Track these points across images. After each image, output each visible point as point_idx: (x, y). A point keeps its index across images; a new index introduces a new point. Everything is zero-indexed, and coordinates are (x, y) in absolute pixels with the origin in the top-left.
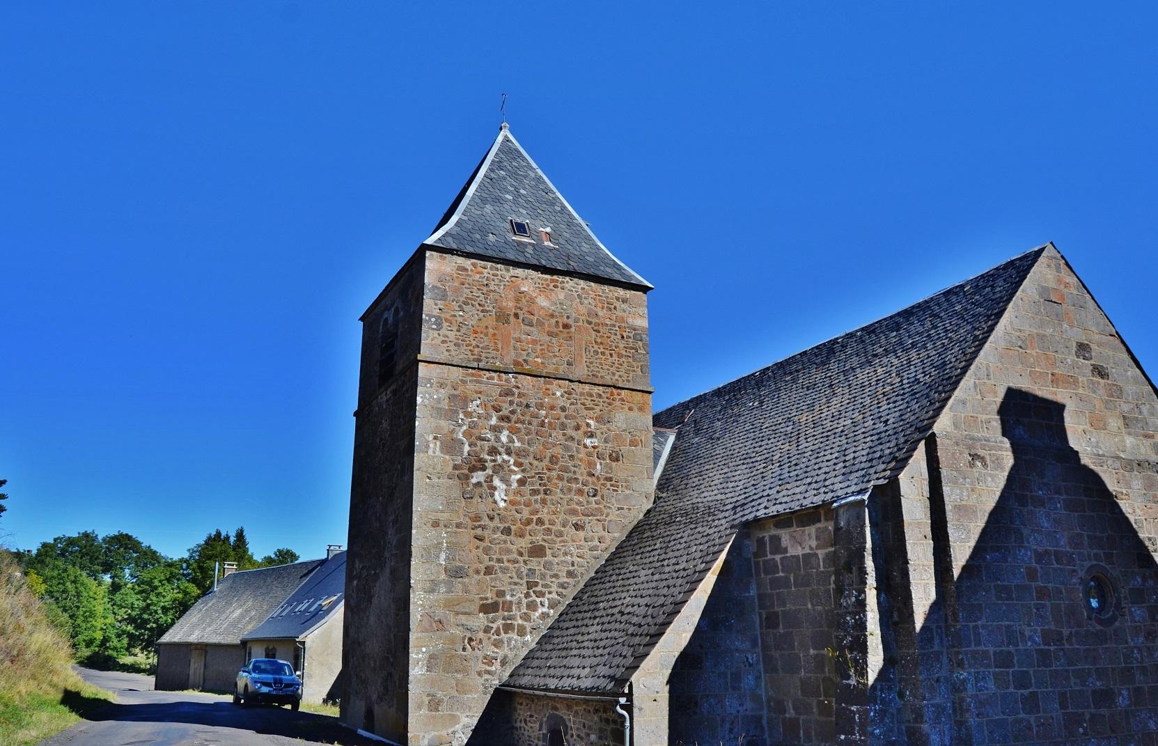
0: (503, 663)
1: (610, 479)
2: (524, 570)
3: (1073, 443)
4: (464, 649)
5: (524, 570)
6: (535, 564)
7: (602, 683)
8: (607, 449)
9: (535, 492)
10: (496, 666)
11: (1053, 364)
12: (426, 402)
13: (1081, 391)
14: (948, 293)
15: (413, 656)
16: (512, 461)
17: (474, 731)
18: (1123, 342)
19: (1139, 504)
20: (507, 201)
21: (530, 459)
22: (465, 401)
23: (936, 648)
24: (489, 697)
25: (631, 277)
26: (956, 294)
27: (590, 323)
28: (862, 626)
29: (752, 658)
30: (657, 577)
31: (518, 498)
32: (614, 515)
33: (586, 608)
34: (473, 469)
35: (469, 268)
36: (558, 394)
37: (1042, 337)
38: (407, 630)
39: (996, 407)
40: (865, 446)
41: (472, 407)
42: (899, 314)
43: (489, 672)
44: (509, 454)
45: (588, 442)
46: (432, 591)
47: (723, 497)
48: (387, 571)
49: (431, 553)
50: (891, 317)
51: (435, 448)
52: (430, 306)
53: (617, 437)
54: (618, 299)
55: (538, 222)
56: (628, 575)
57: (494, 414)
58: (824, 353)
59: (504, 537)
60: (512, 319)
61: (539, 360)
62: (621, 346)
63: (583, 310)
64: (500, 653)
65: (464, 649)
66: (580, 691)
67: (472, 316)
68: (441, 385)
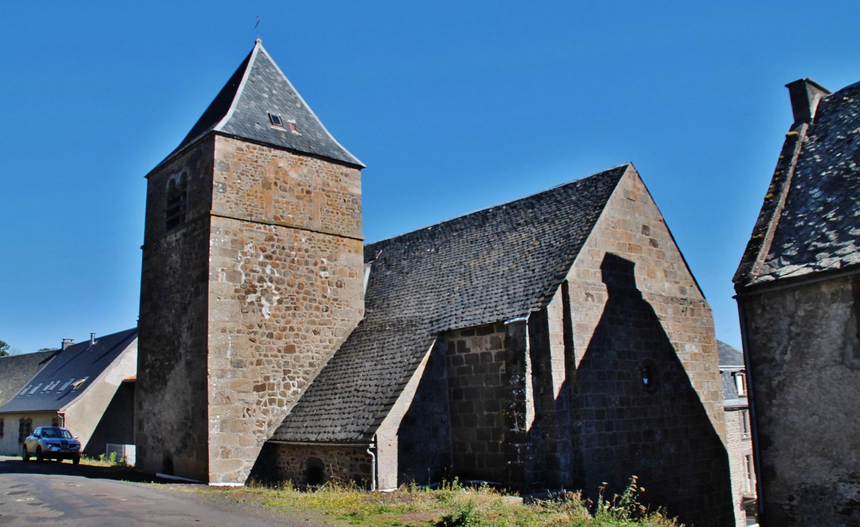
0: (269, 425)
1: (336, 300)
2: (282, 362)
3: (638, 287)
4: (244, 416)
5: (282, 362)
6: (289, 358)
7: (354, 436)
8: (334, 279)
9: (288, 308)
10: (265, 428)
11: (630, 238)
12: (217, 244)
13: (643, 255)
14: (565, 187)
15: (211, 421)
16: (273, 287)
17: (252, 471)
18: (666, 225)
19: (670, 323)
20: (264, 98)
21: (285, 286)
22: (242, 244)
23: (564, 408)
24: (260, 448)
25: (350, 159)
26: (571, 188)
27: (324, 190)
28: (523, 396)
29: (444, 418)
30: (379, 367)
31: (278, 313)
32: (338, 324)
33: (326, 387)
34: (248, 292)
35: (245, 149)
36: (303, 240)
37: (625, 221)
38: (207, 403)
39: (599, 264)
40: (521, 286)
41: (247, 248)
42: (532, 197)
43: (260, 431)
44: (271, 281)
45: (322, 274)
46: (222, 377)
47: (420, 314)
48: (182, 363)
49: (220, 350)
50: (527, 199)
51: (222, 277)
52: (218, 175)
53: (341, 270)
54: (342, 174)
55: (286, 115)
56: (355, 366)
57: (261, 253)
58: (480, 218)
59: (268, 339)
60: (273, 186)
61: (291, 216)
62: (344, 207)
63: (319, 181)
64: (267, 418)
65: (244, 416)
66: (337, 441)
67: (246, 184)
68: (227, 233)
